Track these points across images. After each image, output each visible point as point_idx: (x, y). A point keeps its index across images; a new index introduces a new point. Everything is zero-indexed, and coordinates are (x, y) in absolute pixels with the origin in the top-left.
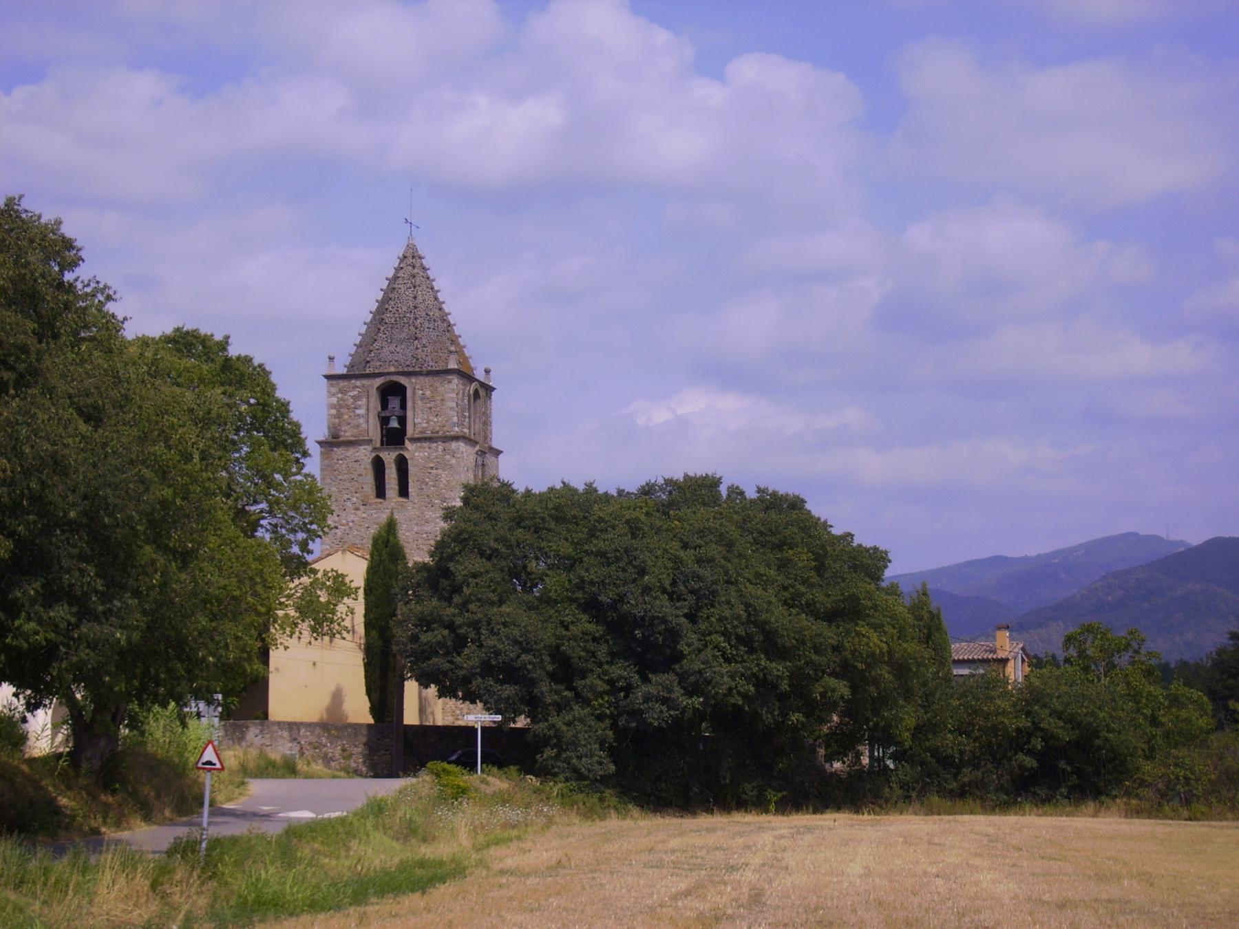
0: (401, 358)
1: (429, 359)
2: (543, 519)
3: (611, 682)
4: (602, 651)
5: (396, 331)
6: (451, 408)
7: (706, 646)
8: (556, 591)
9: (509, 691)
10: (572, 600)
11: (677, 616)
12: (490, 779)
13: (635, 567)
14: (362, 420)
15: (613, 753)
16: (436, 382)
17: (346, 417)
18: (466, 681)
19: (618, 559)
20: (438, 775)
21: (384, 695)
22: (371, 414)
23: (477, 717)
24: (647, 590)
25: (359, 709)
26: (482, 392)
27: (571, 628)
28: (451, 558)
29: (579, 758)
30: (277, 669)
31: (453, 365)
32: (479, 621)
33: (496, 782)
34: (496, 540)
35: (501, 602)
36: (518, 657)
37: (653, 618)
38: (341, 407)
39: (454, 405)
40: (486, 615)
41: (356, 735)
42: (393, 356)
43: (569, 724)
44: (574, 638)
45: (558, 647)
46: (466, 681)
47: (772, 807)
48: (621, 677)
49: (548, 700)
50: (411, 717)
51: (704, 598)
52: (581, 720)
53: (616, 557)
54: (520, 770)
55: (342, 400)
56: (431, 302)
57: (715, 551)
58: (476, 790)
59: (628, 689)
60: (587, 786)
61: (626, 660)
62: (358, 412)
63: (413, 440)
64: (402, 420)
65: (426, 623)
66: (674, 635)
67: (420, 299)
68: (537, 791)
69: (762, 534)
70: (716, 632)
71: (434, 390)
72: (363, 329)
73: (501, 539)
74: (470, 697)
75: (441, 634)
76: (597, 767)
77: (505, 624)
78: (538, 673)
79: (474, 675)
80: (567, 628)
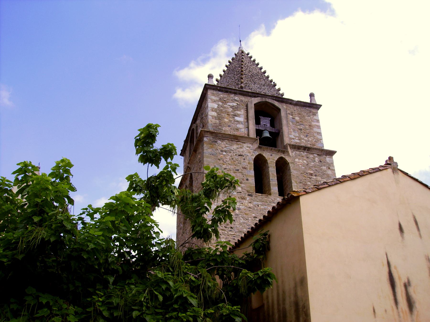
62: (237, 118)
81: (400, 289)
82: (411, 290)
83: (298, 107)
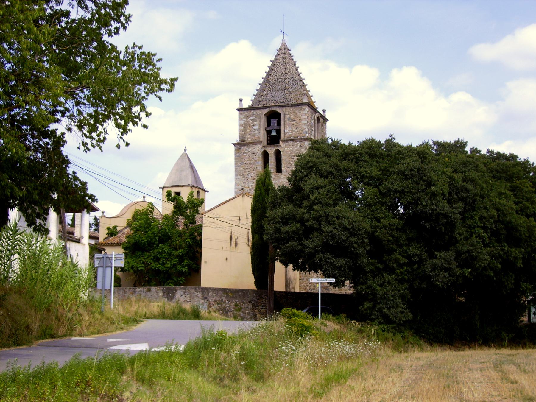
0: (277, 99)
1: (293, 99)
2: (361, 154)
3: (409, 257)
4: (403, 240)
5: (275, 86)
6: (304, 124)
7: (471, 235)
8: (371, 198)
9: (341, 262)
10: (383, 204)
11: (455, 213)
12: (328, 323)
13: (424, 181)
14: (257, 132)
15: (410, 306)
16: (296, 109)
17: (248, 130)
18: (312, 256)
19: (412, 176)
20: (289, 318)
21: (262, 269)
22: (262, 129)
23: (318, 282)
24: (434, 195)
25: (248, 281)
26: (321, 119)
27: (382, 220)
28: (301, 179)
29: (389, 308)
30: (206, 262)
31: (305, 101)
32: (321, 216)
33: (332, 325)
34: (330, 166)
35: (335, 205)
36: (347, 239)
37: (439, 214)
38: (246, 125)
39: (306, 117)
40: (325, 213)
41: (244, 296)
42: (274, 98)
43: (381, 285)
44: (384, 227)
45: (374, 233)
46: (312, 256)
47: (506, 343)
48: (416, 255)
49: (367, 269)
50: (279, 285)
51: (471, 206)
52: (389, 283)
53: (412, 175)
54: (347, 317)
55: (246, 121)
56: (294, 71)
57: (474, 174)
58: (318, 329)
59: (421, 262)
60: (394, 328)
61: (418, 243)
62: (255, 127)
63: (284, 141)
64: (278, 132)
65: (285, 221)
66: (451, 225)
67: (288, 69)
68: (360, 331)
69: (498, 172)
70: (478, 227)
71: (295, 115)
72: (258, 87)
73: (335, 166)
74: (315, 268)
75: (293, 227)
76: (400, 315)
77: (338, 218)
78: (361, 250)
79: (317, 252)
80: (379, 221)
81: (234, 240)
82: (237, 241)
83: (293, 107)
